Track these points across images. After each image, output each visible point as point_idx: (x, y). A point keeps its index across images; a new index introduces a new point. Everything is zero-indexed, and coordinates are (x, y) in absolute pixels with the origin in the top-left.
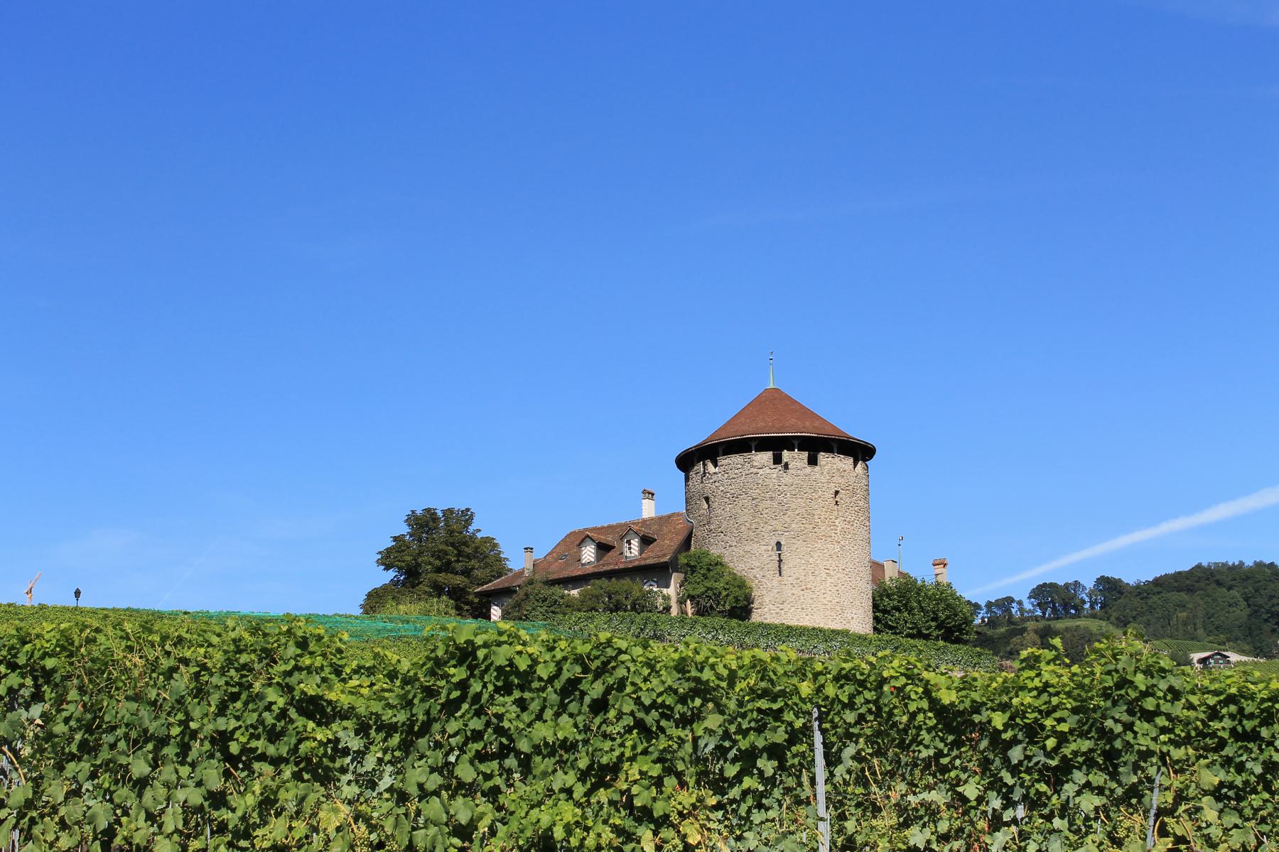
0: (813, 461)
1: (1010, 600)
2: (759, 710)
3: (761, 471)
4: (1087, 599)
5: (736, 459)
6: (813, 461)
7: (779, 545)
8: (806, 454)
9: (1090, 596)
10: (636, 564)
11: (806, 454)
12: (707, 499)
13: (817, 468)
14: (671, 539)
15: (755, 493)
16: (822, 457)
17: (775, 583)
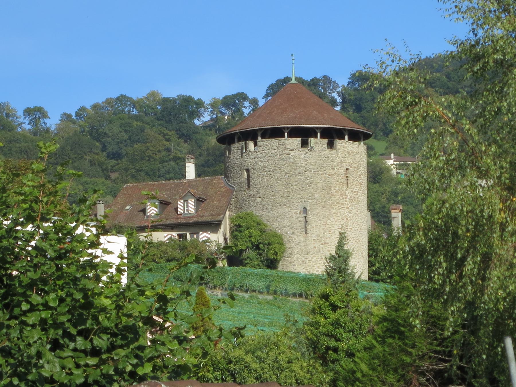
0: (331, 145)
1: (243, 97)
2: (410, 354)
3: (292, 153)
4: (339, 99)
5: (272, 143)
6: (331, 145)
7: (305, 210)
8: (326, 141)
9: (342, 94)
10: (195, 220)
11: (326, 141)
12: (248, 171)
13: (334, 151)
14: (219, 200)
15: (287, 169)
16: (339, 143)
17: (302, 238)
